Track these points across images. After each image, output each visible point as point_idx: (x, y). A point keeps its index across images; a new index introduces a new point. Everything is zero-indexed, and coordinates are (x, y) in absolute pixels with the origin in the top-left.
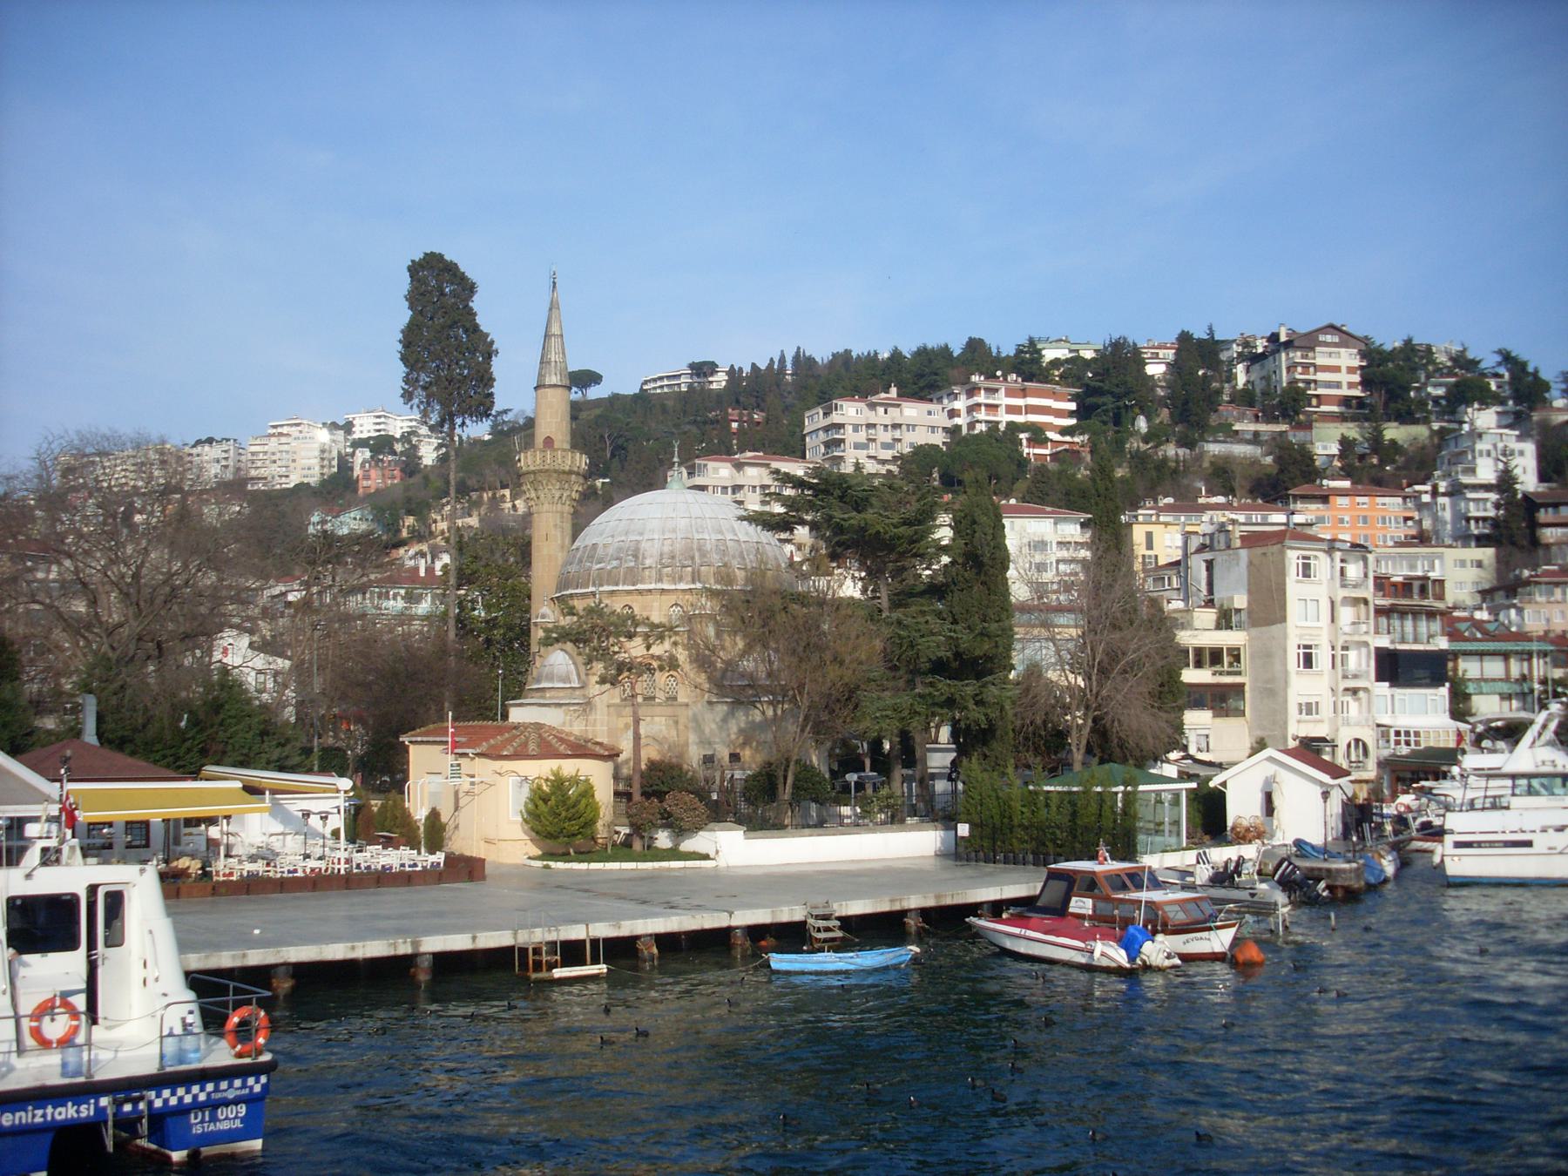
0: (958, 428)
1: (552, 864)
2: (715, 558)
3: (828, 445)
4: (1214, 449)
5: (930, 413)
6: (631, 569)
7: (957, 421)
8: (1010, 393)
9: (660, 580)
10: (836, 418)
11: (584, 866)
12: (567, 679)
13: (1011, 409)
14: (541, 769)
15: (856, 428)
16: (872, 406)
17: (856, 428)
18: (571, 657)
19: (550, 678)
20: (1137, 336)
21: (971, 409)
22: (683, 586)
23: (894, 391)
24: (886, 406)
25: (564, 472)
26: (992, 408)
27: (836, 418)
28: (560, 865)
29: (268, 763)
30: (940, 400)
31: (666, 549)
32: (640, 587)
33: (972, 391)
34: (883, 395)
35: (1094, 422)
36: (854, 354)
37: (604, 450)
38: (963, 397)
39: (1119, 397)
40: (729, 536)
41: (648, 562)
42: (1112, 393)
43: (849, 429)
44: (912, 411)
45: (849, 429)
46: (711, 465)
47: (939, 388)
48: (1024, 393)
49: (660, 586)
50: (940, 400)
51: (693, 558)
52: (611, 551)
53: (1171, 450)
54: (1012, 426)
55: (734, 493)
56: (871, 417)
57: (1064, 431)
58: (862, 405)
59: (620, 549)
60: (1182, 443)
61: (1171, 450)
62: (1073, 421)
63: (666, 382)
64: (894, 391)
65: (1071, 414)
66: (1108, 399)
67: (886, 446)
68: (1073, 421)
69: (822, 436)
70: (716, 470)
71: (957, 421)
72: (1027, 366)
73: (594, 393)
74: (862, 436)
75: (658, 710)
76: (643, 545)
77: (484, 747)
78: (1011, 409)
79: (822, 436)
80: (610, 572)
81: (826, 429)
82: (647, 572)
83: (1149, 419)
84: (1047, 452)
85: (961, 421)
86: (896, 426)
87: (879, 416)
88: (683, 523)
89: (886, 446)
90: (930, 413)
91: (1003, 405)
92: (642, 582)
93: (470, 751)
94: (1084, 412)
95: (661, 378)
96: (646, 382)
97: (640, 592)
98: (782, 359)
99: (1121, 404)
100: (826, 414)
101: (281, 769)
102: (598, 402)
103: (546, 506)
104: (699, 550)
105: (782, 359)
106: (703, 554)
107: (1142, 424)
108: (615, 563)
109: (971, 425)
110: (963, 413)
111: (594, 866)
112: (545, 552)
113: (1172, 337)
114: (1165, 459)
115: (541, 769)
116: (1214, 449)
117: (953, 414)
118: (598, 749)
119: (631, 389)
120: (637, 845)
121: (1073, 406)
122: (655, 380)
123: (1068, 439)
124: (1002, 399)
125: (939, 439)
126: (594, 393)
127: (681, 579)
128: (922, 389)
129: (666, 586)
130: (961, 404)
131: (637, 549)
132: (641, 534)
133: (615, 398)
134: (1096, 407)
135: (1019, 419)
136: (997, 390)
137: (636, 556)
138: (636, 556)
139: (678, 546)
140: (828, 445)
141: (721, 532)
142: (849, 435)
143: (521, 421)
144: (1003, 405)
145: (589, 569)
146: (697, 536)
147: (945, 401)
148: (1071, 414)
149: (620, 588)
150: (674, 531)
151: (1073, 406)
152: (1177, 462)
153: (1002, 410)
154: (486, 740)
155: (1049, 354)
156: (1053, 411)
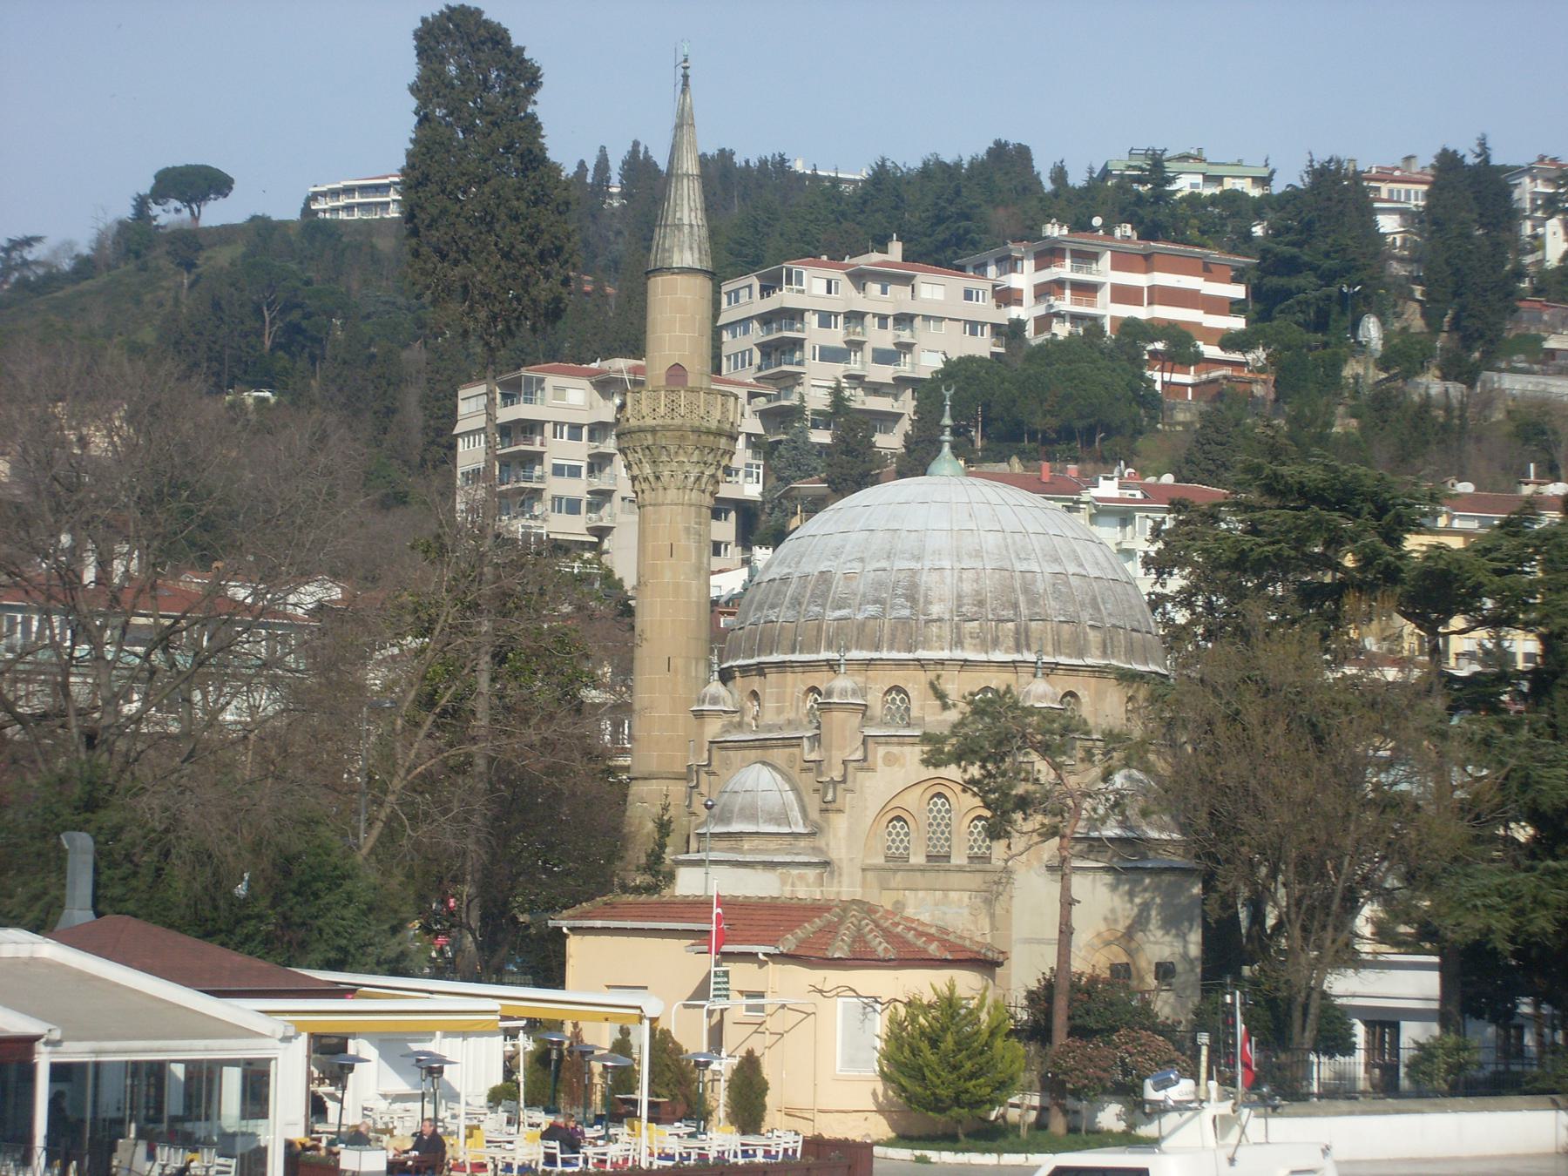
0: (1017, 326)
1: (933, 1155)
2: (1052, 606)
3: (767, 349)
4: (1514, 384)
5: (968, 295)
6: (904, 621)
7: (1015, 312)
8: (1122, 261)
9: (958, 643)
10: (785, 297)
11: (990, 1159)
12: (782, 817)
13: (1123, 294)
14: (924, 984)
15: (826, 319)
16: (860, 279)
17: (826, 319)
18: (787, 778)
19: (750, 814)
20: (1365, 154)
21: (1043, 291)
22: (998, 656)
23: (896, 250)
24: (886, 278)
25: (709, 432)
26: (1086, 290)
27: (785, 297)
28: (948, 1157)
29: (378, 963)
30: (980, 269)
31: (967, 587)
32: (921, 654)
33: (1048, 254)
34: (876, 257)
35: (1285, 324)
36: (739, 160)
37: (260, 334)
38: (1029, 265)
39: (1329, 278)
40: (1072, 568)
41: (936, 610)
42: (1314, 268)
43: (812, 321)
44: (935, 290)
45: (812, 321)
46: (551, 381)
47: (975, 245)
48: (1147, 262)
49: (958, 654)
50: (980, 269)
51: (1015, 606)
52: (861, 586)
53: (1432, 384)
54: (1130, 329)
55: (591, 438)
56: (848, 297)
57: (1229, 341)
58: (837, 274)
59: (880, 585)
60: (1455, 369)
61: (1432, 384)
62: (1238, 323)
63: (358, 199)
64: (896, 250)
65: (1234, 307)
66: (1306, 280)
67: (882, 357)
68: (1238, 323)
69: (757, 334)
70: (560, 389)
71: (1015, 312)
72: (1144, 208)
73: (215, 214)
74: (836, 336)
75: (955, 879)
76: (926, 579)
77: (788, 944)
78: (1123, 294)
79: (757, 334)
80: (863, 624)
81: (767, 319)
82: (934, 628)
83: (1383, 323)
84: (1188, 379)
85: (1026, 312)
86: (904, 320)
87: (875, 299)
88: (991, 541)
89: (882, 357)
90: (968, 295)
91: (1116, 289)
92: (926, 645)
93: (760, 950)
94: (1263, 304)
95: (349, 191)
96: (314, 197)
97: (921, 664)
98: (603, 165)
99: (1334, 290)
100: (766, 290)
101: (394, 972)
102: (226, 234)
103: (672, 494)
104: (1026, 591)
105: (603, 165)
106: (1033, 601)
107: (1371, 330)
108: (872, 609)
109: (1043, 323)
110: (1028, 296)
111: (1010, 1159)
112: (667, 577)
113: (1426, 159)
114: (1427, 402)
115: (924, 984)
116: (1514, 384)
117: (1006, 297)
118: (933, 949)
119: (287, 210)
120: (1058, 1124)
121: (1238, 292)
122: (335, 193)
123: (1237, 357)
124: (1105, 273)
125: (983, 346)
126: (215, 214)
127: (996, 643)
128: (945, 244)
129: (971, 656)
130: (1024, 279)
131: (913, 586)
132: (918, 559)
133: (262, 228)
134: (1287, 294)
135: (1142, 313)
136: (1094, 257)
137: (912, 598)
138: (912, 598)
139: (989, 584)
140: (767, 349)
141: (1057, 560)
142: (813, 334)
143: (66, 265)
144: (1116, 289)
145: (818, 618)
146: (1019, 566)
147: (992, 271)
148: (1234, 307)
149: (885, 654)
150: (978, 554)
151: (1238, 292)
152: (1448, 409)
153: (1104, 295)
154: (790, 930)
155: (1185, 184)
156: (1203, 300)
